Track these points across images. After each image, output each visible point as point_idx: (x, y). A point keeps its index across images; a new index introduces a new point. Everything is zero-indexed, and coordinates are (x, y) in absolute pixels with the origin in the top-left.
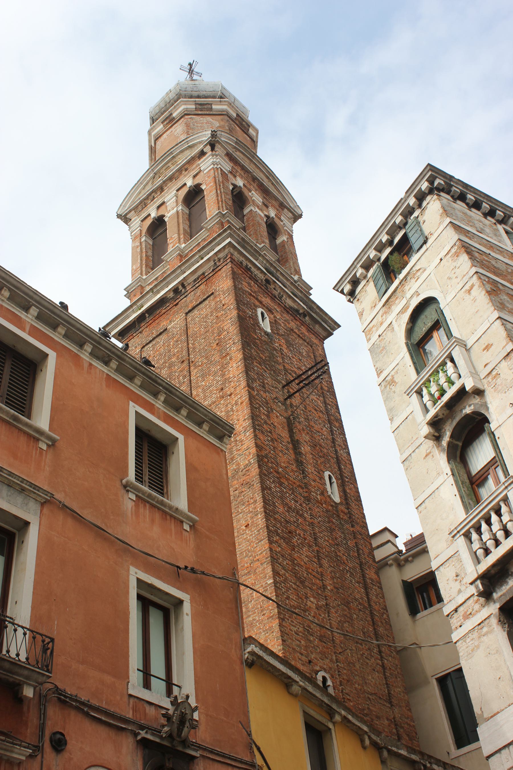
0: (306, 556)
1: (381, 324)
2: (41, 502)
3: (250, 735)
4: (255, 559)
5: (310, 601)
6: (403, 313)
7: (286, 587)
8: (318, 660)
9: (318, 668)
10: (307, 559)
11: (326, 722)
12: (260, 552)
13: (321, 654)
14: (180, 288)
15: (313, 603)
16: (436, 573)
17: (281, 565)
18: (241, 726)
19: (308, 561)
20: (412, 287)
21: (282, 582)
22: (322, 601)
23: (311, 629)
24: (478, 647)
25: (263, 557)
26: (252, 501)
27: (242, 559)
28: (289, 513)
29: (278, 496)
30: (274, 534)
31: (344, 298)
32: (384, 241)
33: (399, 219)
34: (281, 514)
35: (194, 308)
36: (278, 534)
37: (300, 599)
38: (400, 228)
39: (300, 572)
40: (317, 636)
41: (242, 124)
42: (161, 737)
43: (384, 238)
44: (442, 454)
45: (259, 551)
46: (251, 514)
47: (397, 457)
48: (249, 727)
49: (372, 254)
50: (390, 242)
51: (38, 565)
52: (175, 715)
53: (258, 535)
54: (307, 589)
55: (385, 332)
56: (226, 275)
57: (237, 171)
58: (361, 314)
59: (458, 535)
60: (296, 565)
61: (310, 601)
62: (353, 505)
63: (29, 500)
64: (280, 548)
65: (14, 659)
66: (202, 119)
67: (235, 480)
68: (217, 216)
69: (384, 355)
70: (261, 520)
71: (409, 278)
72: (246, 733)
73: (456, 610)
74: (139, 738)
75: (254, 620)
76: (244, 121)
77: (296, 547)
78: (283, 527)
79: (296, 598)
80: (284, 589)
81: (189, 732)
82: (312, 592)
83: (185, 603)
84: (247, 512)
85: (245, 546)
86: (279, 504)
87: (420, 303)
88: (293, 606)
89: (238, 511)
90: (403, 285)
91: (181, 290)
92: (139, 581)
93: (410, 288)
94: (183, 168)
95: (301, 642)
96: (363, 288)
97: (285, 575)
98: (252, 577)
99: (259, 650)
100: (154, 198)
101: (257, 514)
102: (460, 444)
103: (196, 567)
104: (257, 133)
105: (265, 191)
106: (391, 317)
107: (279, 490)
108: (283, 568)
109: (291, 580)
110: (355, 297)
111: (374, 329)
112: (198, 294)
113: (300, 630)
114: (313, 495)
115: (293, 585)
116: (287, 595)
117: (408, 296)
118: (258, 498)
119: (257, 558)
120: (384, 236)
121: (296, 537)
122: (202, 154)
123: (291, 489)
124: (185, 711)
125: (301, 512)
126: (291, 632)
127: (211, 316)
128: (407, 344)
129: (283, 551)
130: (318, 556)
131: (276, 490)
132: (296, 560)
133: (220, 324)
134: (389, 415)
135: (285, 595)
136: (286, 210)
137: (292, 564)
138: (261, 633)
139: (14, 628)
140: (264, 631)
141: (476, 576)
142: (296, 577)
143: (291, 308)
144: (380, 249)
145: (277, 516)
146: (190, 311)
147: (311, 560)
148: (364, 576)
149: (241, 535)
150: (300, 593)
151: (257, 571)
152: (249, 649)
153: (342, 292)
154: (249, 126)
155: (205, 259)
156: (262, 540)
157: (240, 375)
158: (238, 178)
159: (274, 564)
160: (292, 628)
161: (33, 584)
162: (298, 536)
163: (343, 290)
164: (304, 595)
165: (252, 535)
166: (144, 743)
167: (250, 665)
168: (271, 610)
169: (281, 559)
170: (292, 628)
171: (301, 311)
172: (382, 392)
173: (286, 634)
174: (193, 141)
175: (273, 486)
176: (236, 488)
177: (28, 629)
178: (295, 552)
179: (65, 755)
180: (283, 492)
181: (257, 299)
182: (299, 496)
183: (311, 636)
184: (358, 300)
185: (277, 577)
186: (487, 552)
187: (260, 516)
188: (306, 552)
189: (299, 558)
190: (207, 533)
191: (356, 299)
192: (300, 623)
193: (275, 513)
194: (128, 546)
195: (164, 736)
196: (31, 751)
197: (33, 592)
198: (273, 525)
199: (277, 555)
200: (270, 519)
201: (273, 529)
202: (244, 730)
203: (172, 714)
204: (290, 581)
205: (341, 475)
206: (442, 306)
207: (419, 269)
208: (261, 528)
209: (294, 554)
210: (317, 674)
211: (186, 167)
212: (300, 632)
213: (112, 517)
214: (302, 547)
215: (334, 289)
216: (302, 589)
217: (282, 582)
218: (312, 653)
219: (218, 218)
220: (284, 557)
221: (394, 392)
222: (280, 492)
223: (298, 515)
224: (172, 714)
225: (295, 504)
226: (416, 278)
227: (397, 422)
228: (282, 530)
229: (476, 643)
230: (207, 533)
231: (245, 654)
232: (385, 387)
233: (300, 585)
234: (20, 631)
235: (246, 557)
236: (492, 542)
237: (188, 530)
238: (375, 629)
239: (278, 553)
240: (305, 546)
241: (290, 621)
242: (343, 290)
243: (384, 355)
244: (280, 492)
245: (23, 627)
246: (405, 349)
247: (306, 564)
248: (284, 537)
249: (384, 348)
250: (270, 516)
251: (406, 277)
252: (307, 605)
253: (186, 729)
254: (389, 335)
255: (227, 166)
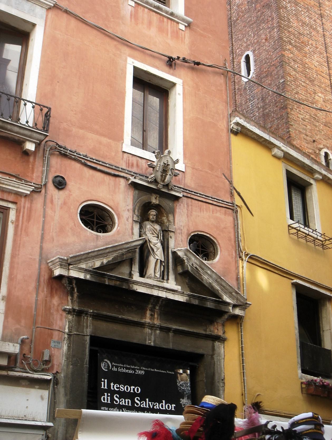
0: (317, 62)
2: (46, 8)
3: (231, 183)
4: (271, 65)
5: (318, 96)
7: (296, 84)
8: (322, 141)
9: (322, 146)
10: (317, 63)
11: (308, 179)
12: (275, 59)
13: (325, 136)
15: (321, 98)
17: (292, 68)
18: (224, 177)
19: (318, 65)
21: (292, 81)
22: (329, 96)
23: (317, 117)
25: (277, 62)
26: (270, 19)
27: (262, 65)
28: (304, 28)
29: (293, 14)
30: (288, 43)
34: (294, 28)
36: (291, 44)
37: (309, 94)
39: (309, 74)
40: (323, 122)
42: (148, 182)
45: (275, 57)
46: (269, 29)
48: (231, 177)
51: (43, 56)
52: (159, 165)
53: (274, 45)
54: (315, 87)
60: (307, 68)
61: (318, 96)
63: (36, 7)
64: (292, 55)
65: (24, 125)
67: (258, 4)
70: (277, 33)
72: (228, 182)
74: (130, 182)
75: (270, 111)
77: (308, 54)
78: (296, 38)
79: (304, 93)
80: (294, 86)
81: (172, 178)
82: (320, 89)
83: (177, 86)
84: (266, 29)
85: (265, 55)
86: (293, 20)
88: (301, 99)
89: (260, 28)
92: (135, 68)
95: (307, 127)
97: (295, 75)
98: (269, 79)
99: (243, 122)
101: (274, 29)
103: (187, 58)
107: (294, 9)
108: (295, 70)
109: (301, 79)
113: (306, 118)
114: (327, 13)
115: (303, 83)
116: (296, 91)
118: (275, 16)
119: (273, 63)
121: (309, 47)
123: (306, 8)
124: (167, 163)
125: (314, 26)
126: (298, 119)
129: (295, 57)
130: (328, 61)
131: (291, 9)
132: (307, 64)
135: (295, 91)
137: (302, 67)
138: (274, 120)
139: (40, 108)
140: (277, 119)
142: (305, 77)
145: (291, 30)
147: (321, 64)
149: (261, 47)
150: (309, 90)
151: (273, 73)
152: (234, 121)
156: (277, 49)
159: (286, 67)
160: (299, 115)
161: (38, 70)
162: (311, 46)
164: (312, 91)
165: (269, 46)
166: (134, 185)
167: (236, 133)
168: (283, 102)
169: (293, 63)
170: (299, 115)
173: (294, 120)
175: (288, 5)
176: (259, 10)
177: (36, 104)
178: (307, 58)
180: (299, 10)
182: (313, 14)
183: (317, 122)
185: (288, 77)
187: (276, 30)
188: (317, 58)
189: (310, 62)
190: (202, 32)
192: (307, 112)
193: (289, 27)
194: (105, 31)
195: (150, 181)
196: (34, 188)
197: (39, 76)
198: (287, 37)
199: (289, 60)
200: (284, 31)
201: (286, 40)
202: (227, 180)
203: (156, 165)
204: (300, 80)
208: (276, 40)
209: (306, 59)
210: (320, 151)
212: (307, 119)
213: (112, 20)
214: (313, 54)
216: (311, 86)
217: (292, 81)
218: (317, 135)
220: (295, 62)
222: (295, 10)
223: (312, 29)
224: (156, 165)
225: (309, 20)
228: (295, 41)
230: (202, 32)
231: (231, 125)
233: (310, 84)
234: (29, 105)
235: (265, 64)
237: (184, 29)
239: (290, 58)
240: (316, 54)
241: (298, 111)
244: (295, 10)
245: (31, 102)
247: (316, 67)
248: (296, 46)
250: (284, 29)
252: (315, 99)
253: (168, 177)
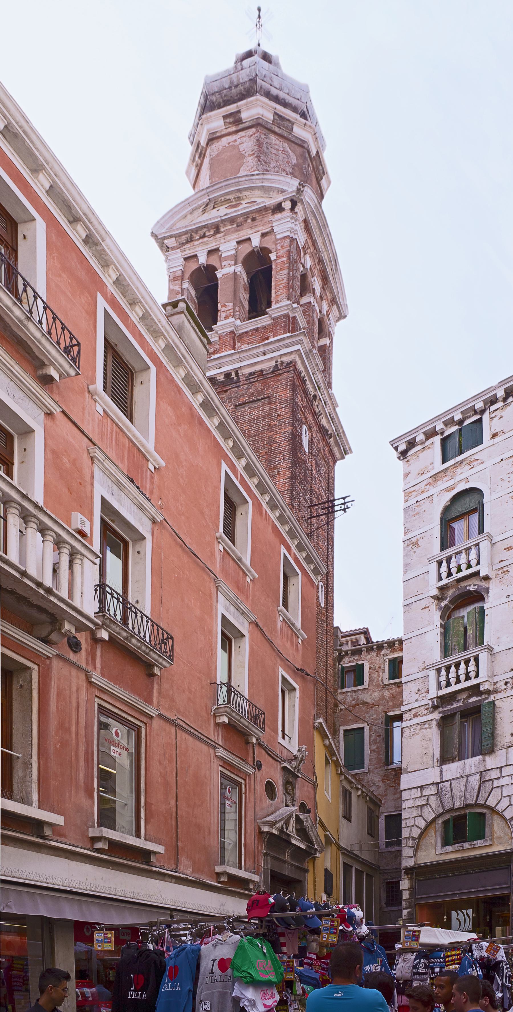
1: (423, 492)
6: (447, 491)
14: (233, 375)
16: (404, 685)
20: (464, 472)
24: (417, 734)
31: (395, 454)
32: (456, 419)
33: (479, 405)
35: (245, 403)
38: (476, 412)
41: (318, 168)
43: (458, 416)
44: (438, 611)
47: (400, 601)
49: (440, 426)
50: (461, 422)
55: (424, 501)
56: (286, 384)
57: (309, 248)
58: (406, 475)
59: (432, 668)
62: (329, 609)
66: (277, 142)
68: (286, 308)
69: (416, 519)
71: (464, 463)
73: (410, 710)
76: (321, 165)
87: (466, 489)
90: (457, 467)
91: (233, 378)
93: (462, 473)
94: (250, 215)
96: (416, 452)
100: (204, 236)
102: (452, 607)
104: (328, 186)
105: (325, 280)
106: (434, 490)
110: (406, 458)
111: (414, 493)
112: (252, 390)
117: (458, 478)
120: (458, 414)
122: (278, 208)
127: (263, 420)
128: (441, 519)
133: (272, 433)
134: (404, 568)
136: (335, 306)
141: (436, 696)
143: (323, 427)
144: (447, 424)
146: (240, 405)
148: (327, 662)
153: (396, 448)
154: (324, 173)
155: (268, 356)
157: (286, 492)
158: (307, 257)
163: (397, 447)
171: (329, 432)
172: (404, 548)
174: (272, 182)
179: (261, 771)
181: (304, 415)
184: (408, 461)
186: (448, 684)
191: (406, 460)
205: (327, 585)
206: (485, 500)
207: (478, 460)
211: (254, 215)
215: (390, 442)
219: (287, 310)
221: (415, 552)
226: (472, 466)
227: (410, 575)
229: (417, 732)
232: (408, 545)
236: (455, 679)
238: (326, 697)
242: (397, 447)
243: (416, 519)
246: (438, 522)
249: (418, 513)
251: (462, 462)
254: (426, 505)
255: (302, 238)
